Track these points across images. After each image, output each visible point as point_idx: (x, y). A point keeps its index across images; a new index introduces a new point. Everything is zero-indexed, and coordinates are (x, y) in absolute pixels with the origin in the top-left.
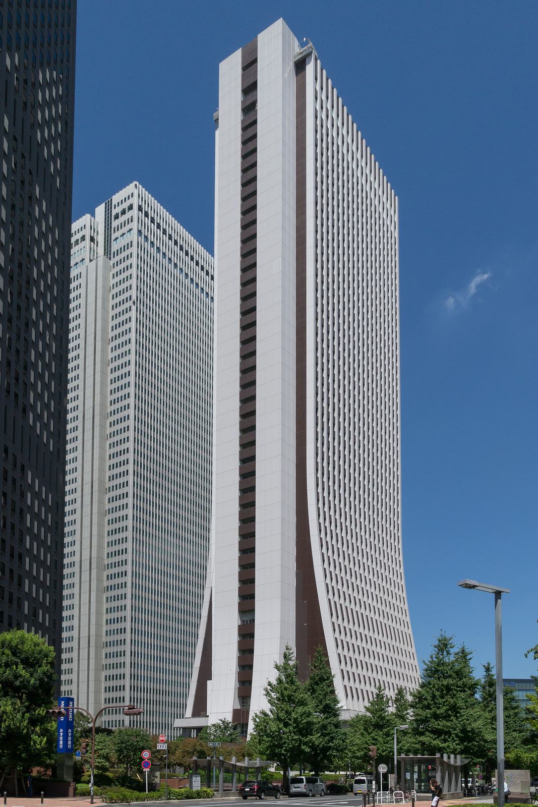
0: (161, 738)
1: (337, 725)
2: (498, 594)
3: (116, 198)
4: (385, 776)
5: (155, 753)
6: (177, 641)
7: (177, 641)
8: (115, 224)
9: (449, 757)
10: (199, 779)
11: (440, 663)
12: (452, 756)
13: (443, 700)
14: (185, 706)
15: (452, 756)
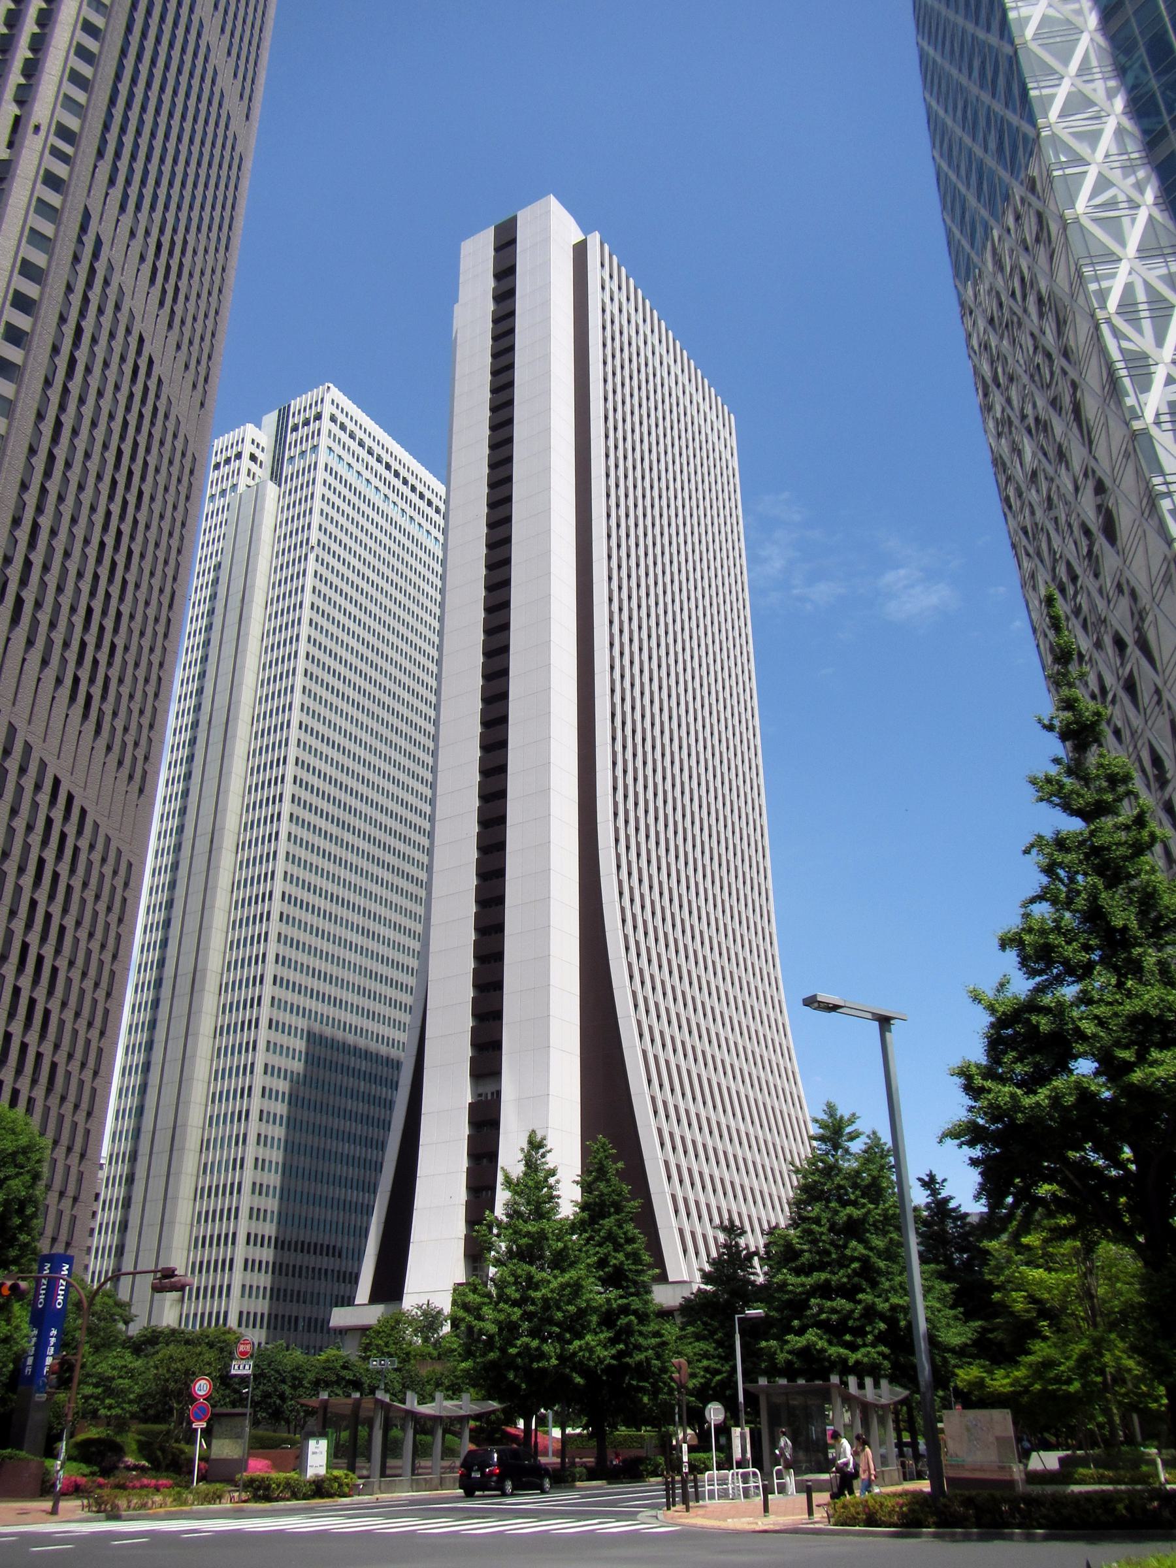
0: (242, 1348)
1: (643, 1318)
2: (884, 1022)
3: (296, 404)
4: (724, 1430)
5: (224, 1380)
6: (350, 1138)
7: (350, 1138)
8: (291, 437)
9: (861, 1386)
10: (323, 1444)
11: (830, 1171)
12: (869, 1381)
13: (833, 1250)
14: (354, 1279)
15: (869, 1381)
